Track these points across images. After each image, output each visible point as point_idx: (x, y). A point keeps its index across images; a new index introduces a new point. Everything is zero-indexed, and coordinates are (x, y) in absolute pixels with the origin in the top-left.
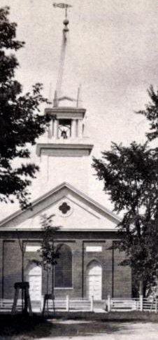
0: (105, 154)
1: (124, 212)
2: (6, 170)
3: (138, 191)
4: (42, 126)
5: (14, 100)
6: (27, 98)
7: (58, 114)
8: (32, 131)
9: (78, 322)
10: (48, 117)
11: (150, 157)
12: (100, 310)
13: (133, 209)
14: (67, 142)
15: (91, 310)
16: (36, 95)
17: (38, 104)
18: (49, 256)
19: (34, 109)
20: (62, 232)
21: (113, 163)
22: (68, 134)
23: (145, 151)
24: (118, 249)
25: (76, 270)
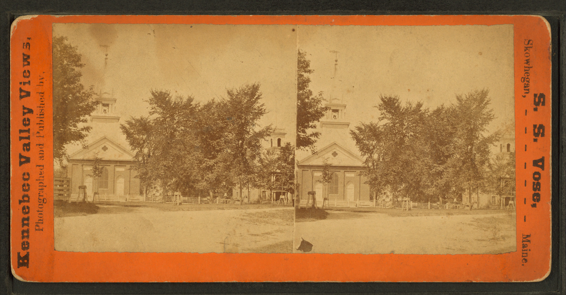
1: (137, 150)
2: (304, 134)
3: (144, 141)
4: (95, 107)
5: (308, 99)
6: (86, 93)
7: (331, 107)
8: (88, 110)
10: (326, 109)
11: (380, 129)
12: (353, 206)
15: (348, 206)
16: (320, 97)
17: (92, 96)
18: (326, 178)
20: (102, 161)
21: (360, 132)
22: (337, 117)
24: (133, 170)
25: (340, 186)
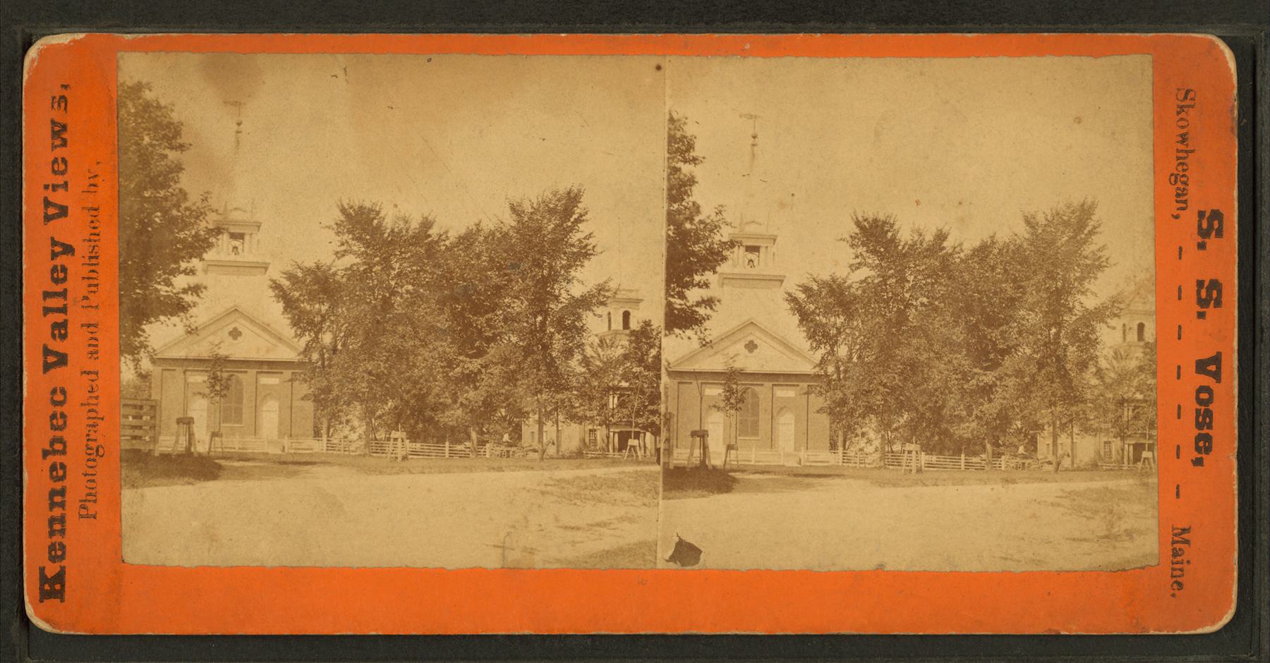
0: (284, 273)
1: (306, 338)
2: (682, 302)
3: (323, 316)
5: (691, 223)
8: (198, 246)
9: (766, 476)
10: (732, 244)
11: (853, 290)
12: (792, 463)
13: (832, 349)
14: (753, 271)
16: (718, 217)
17: (206, 215)
19: (715, 234)
21: (809, 297)
22: (756, 264)
23: (846, 285)
24: (297, 382)
25: (764, 417)
